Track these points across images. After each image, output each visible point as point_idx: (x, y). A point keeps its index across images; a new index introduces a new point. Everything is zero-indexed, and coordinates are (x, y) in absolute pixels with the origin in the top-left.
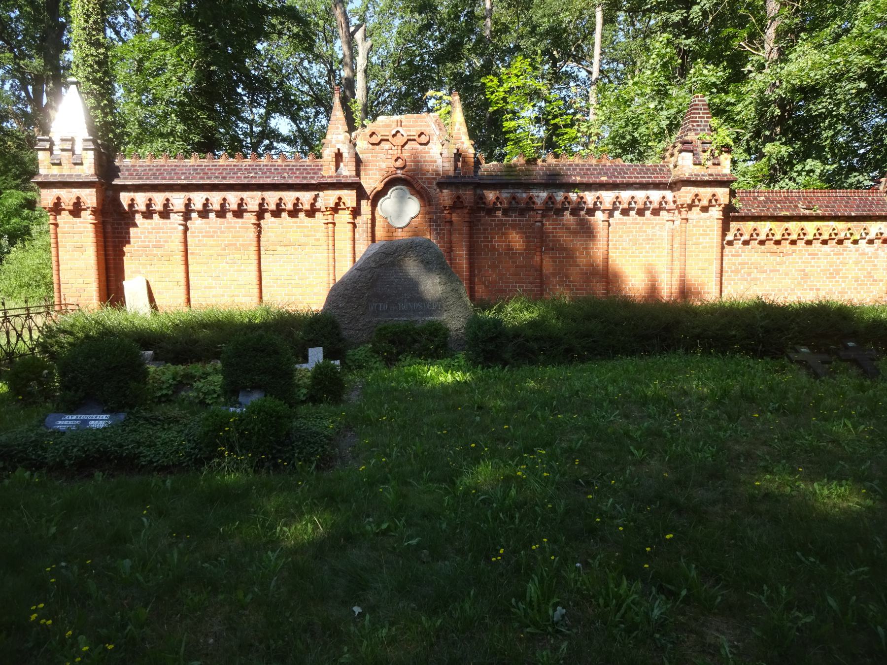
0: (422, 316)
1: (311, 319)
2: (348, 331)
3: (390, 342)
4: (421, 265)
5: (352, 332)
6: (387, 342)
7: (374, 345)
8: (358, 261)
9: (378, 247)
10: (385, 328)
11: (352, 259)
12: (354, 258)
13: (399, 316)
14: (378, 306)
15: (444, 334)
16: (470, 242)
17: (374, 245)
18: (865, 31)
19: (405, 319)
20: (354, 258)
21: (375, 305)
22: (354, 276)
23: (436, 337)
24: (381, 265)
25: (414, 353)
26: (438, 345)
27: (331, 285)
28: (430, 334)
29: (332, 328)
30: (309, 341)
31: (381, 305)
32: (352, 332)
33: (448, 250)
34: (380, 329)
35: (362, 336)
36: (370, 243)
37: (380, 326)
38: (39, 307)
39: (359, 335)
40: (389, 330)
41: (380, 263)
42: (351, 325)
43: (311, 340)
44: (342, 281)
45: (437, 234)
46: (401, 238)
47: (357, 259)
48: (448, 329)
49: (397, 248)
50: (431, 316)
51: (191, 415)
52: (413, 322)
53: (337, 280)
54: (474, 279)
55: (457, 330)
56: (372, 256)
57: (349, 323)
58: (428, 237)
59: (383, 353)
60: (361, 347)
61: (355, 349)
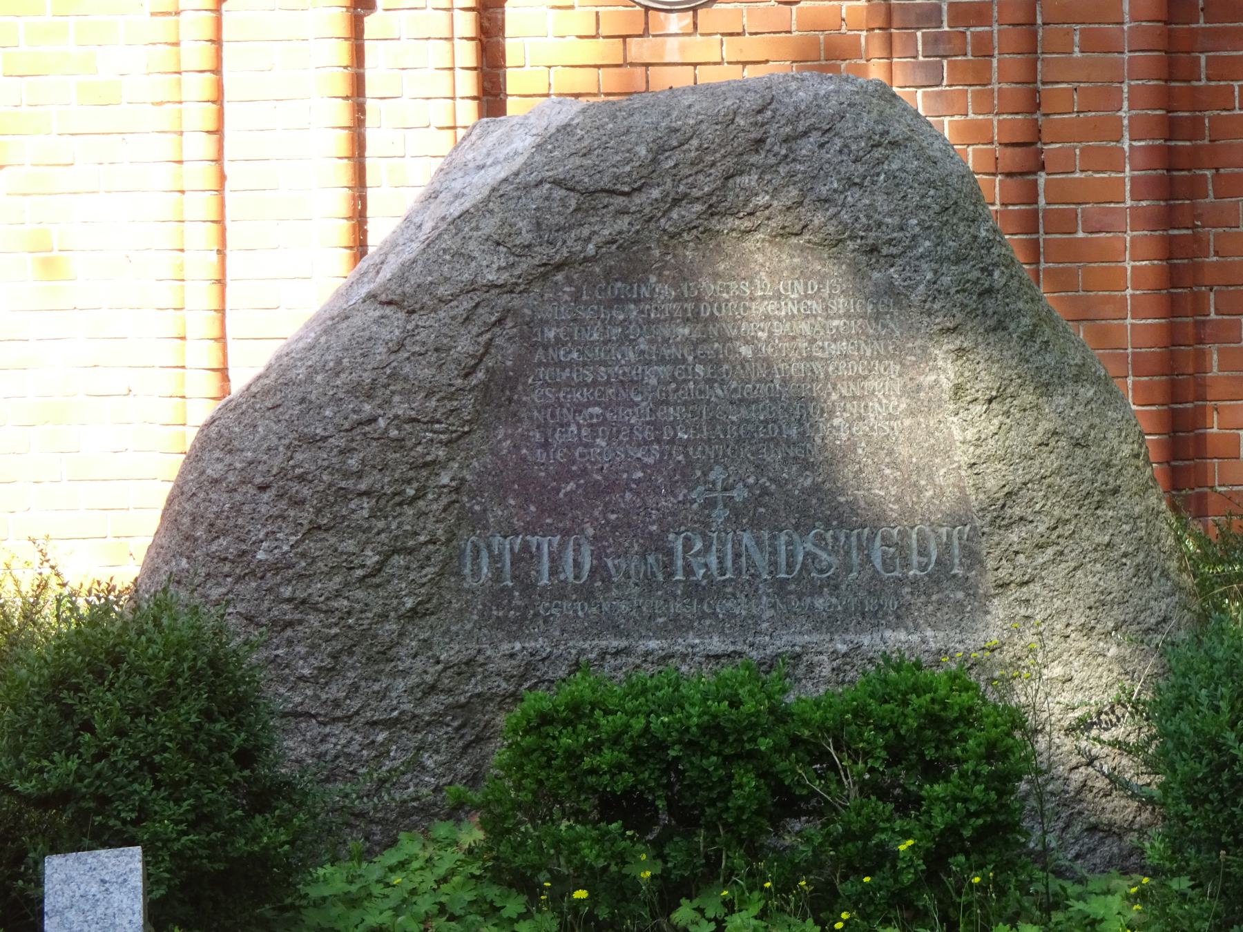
0: (830, 623)
1: (63, 644)
2: (313, 729)
3: (611, 806)
4: (831, 268)
5: (341, 737)
6: (589, 804)
7: (497, 828)
8: (392, 245)
9: (523, 143)
10: (577, 712)
11: (342, 231)
12: (359, 218)
13: (678, 626)
14: (525, 556)
15: (992, 752)
16: (1167, 100)
17: (498, 129)
18: (1136, 834)
19: (716, 644)
20: (359, 218)
21: (506, 546)
22: (362, 345)
23: (933, 771)
24: (550, 269)
25: (785, 886)
26: (952, 830)
27: (202, 411)
28: (896, 755)
29: (207, 715)
30: (43, 802)
31: (546, 544)
32: (341, 737)
33: (1012, 159)
34: (545, 719)
35: (416, 766)
36: (468, 112)
37: (538, 700)
38: (681, 145)
39: (397, 758)
40: (606, 723)
41: (542, 253)
42: (336, 691)
43: (62, 798)
44: (252, 394)
45: (933, 42)
46: (681, 78)
47: (377, 235)
48: (1016, 720)
49: (660, 150)
50: (899, 620)
51: (210, 862)
52: (770, 664)
53: (238, 383)
54: (1201, 357)
55: (1084, 725)
56: (482, 209)
57: (329, 673)
58: (876, 71)
59: (563, 885)
60: (409, 845)
61: (368, 855)
